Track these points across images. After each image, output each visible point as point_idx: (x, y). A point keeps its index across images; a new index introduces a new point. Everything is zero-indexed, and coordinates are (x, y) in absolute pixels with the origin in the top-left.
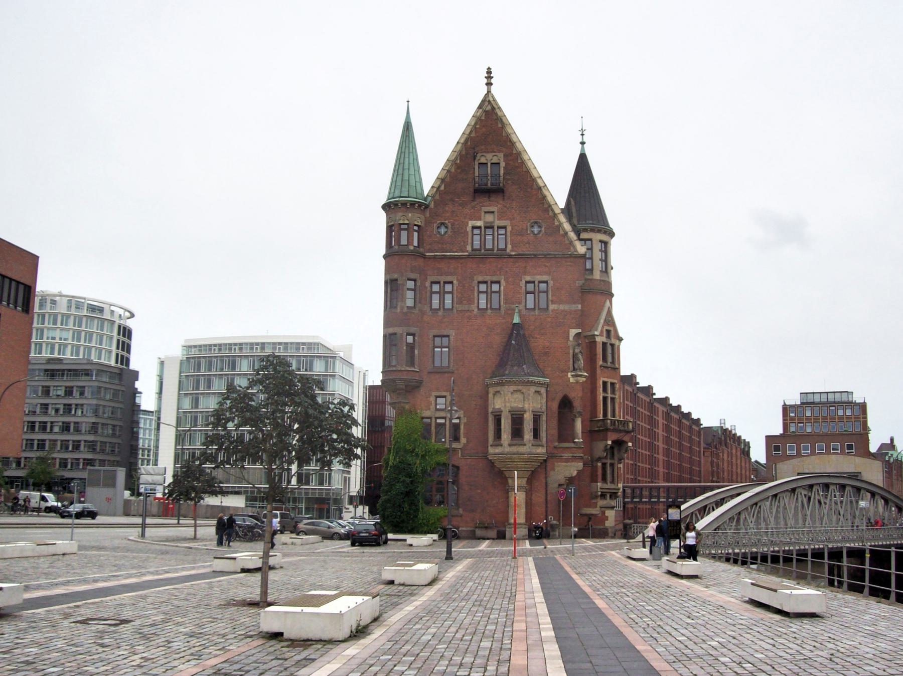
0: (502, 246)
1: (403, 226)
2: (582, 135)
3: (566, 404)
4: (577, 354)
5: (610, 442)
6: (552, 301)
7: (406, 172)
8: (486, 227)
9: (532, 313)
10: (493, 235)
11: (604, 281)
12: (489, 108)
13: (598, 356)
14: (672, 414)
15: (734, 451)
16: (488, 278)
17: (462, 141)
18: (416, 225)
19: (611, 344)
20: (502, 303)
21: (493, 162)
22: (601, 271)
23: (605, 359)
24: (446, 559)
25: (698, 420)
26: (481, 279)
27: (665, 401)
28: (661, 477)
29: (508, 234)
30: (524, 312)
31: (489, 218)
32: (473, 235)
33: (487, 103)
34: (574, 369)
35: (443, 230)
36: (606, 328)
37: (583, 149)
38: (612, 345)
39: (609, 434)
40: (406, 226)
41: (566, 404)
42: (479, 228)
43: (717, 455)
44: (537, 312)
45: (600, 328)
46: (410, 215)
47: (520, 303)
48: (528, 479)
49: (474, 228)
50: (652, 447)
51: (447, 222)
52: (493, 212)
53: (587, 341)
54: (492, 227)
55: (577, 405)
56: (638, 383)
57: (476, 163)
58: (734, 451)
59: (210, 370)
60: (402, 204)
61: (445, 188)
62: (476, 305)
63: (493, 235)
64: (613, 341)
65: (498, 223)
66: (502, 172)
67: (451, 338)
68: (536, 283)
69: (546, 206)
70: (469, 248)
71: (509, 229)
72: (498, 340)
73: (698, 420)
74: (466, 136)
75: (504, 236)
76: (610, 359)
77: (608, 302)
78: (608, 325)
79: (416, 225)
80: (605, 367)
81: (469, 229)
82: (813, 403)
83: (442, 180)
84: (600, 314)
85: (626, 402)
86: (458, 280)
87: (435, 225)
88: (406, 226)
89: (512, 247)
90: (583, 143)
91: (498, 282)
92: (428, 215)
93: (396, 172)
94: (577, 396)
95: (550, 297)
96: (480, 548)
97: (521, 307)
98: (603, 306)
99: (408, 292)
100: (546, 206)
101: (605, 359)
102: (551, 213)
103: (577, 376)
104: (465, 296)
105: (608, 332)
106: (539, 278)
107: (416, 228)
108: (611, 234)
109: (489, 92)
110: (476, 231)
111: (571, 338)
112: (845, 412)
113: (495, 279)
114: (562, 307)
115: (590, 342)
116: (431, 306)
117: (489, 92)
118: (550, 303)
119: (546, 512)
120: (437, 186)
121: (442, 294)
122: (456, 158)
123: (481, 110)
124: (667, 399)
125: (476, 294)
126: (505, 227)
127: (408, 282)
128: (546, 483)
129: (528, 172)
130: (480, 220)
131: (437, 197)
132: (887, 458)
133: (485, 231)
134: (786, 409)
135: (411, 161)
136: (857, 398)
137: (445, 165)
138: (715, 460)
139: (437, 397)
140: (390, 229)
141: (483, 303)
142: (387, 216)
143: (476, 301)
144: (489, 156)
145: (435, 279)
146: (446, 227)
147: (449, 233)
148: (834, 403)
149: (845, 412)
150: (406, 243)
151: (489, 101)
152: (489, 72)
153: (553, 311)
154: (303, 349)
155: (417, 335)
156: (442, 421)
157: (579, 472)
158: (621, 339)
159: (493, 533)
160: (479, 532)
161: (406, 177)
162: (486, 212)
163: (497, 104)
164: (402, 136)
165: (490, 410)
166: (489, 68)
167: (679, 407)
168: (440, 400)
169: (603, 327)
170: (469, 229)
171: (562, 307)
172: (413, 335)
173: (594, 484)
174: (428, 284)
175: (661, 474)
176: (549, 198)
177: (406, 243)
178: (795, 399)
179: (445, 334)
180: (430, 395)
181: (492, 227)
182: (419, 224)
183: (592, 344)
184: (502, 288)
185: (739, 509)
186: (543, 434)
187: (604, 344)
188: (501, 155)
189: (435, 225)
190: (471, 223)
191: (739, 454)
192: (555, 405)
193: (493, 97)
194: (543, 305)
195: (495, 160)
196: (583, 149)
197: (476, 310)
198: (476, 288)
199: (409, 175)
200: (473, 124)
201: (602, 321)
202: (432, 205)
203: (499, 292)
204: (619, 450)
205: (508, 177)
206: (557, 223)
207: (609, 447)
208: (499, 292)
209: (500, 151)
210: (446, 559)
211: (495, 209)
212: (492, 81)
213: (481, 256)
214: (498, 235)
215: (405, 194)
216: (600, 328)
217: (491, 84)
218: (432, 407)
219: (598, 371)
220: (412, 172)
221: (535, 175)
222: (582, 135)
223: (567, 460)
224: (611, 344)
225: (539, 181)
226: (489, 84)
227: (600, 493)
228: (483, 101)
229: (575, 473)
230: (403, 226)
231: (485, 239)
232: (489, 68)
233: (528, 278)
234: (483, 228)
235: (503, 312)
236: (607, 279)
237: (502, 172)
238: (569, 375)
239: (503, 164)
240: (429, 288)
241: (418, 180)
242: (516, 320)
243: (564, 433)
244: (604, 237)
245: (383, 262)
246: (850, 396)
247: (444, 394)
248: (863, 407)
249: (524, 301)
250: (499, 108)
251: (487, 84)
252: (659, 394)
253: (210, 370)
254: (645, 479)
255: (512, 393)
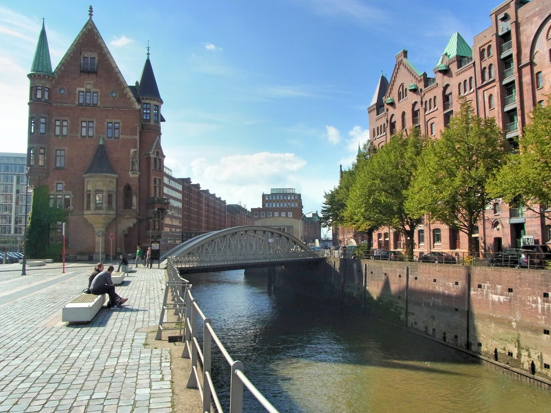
0: (95, 102)
1: (39, 88)
2: (148, 50)
3: (128, 188)
4: (134, 162)
5: (156, 209)
6: (121, 133)
7: (41, 57)
8: (86, 92)
9: (110, 139)
10: (90, 96)
11: (156, 126)
12: (90, 27)
13: (151, 165)
14: (217, 201)
15: (243, 216)
16: (87, 119)
17: (74, 44)
18: (46, 88)
19: (159, 159)
20: (94, 133)
21: (91, 57)
22: (155, 121)
23: (155, 167)
24: (22, 275)
25: (225, 201)
26: (83, 120)
27: (207, 192)
28: (204, 228)
29: (99, 96)
30: (106, 139)
31: (89, 87)
32: (79, 95)
33: (89, 25)
34: (132, 170)
35: (62, 92)
36: (156, 150)
37: (148, 57)
38: (160, 160)
39: (156, 205)
40: (40, 88)
41: (128, 188)
42: (83, 92)
43: (235, 218)
44: (113, 139)
45: (153, 150)
46: (43, 82)
47: (104, 134)
48: (106, 228)
49: (79, 92)
50: (199, 214)
51: (65, 87)
52: (91, 84)
53: (146, 157)
54: (90, 92)
55: (134, 188)
56: (191, 182)
57: (82, 56)
58: (243, 216)
59: (7, 181)
60: (38, 75)
61: (64, 69)
62: (80, 134)
63: (90, 96)
64: (160, 157)
65: (93, 90)
66: (96, 62)
67: (66, 151)
68: (113, 123)
69: (120, 83)
70: (77, 103)
71: (99, 93)
72: (91, 153)
73: (225, 201)
74: (76, 41)
75: (96, 97)
76: (158, 167)
77: (158, 137)
78: (158, 149)
79: (46, 88)
80: (155, 170)
81: (77, 92)
82: (280, 194)
83: (61, 64)
84: (153, 143)
85: (185, 191)
86: (70, 119)
87: (58, 88)
88: (40, 88)
89: (101, 103)
90: (148, 54)
91: (92, 122)
92: (54, 82)
93: (38, 60)
94: (134, 185)
95: (120, 131)
96: (355, 268)
97: (105, 136)
98: (155, 139)
99: (41, 124)
100: (120, 83)
101: (155, 167)
102: (122, 87)
103: (134, 173)
104: (74, 128)
105: (158, 153)
106: (114, 121)
107: (47, 89)
108: (162, 102)
109: (91, 19)
110: (81, 94)
111: (131, 154)
112: (291, 198)
113: (90, 120)
114: (127, 137)
115: (148, 158)
116: (55, 133)
117: (91, 19)
118: (120, 134)
119: (116, 246)
120: (59, 67)
121: (61, 126)
122: (71, 53)
123: (85, 28)
124: (208, 190)
125: (80, 128)
126: (97, 93)
127: (41, 119)
128: (116, 230)
129: (110, 64)
130: (83, 87)
131: (60, 73)
132: (314, 220)
133: (86, 94)
134: (264, 196)
135: (44, 52)
136: (297, 192)
137: (65, 56)
138: (233, 220)
139: (57, 184)
140: (31, 89)
141: (84, 133)
142: (31, 84)
143: (80, 132)
144: (89, 53)
145: (57, 118)
146: (64, 90)
147: (66, 93)
148: (286, 194)
149: (291, 198)
150: (40, 97)
151: (90, 24)
152: (91, 8)
153: (122, 138)
154: (5, 160)
155: (46, 148)
156: (60, 197)
157: (134, 225)
158: (164, 157)
159: (86, 257)
160: (79, 257)
161: (41, 61)
162: (86, 84)
163: (95, 26)
164: (40, 38)
165: (85, 191)
166: (91, 6)
167: (214, 195)
168: (59, 185)
169: (155, 149)
170: (77, 92)
171: (127, 137)
172: (44, 149)
173: (148, 231)
174: (53, 121)
175: (204, 227)
176: (121, 79)
177: (40, 97)
178: (268, 192)
179: (63, 149)
180: (53, 183)
181: (90, 92)
182: (49, 87)
183: (149, 159)
184: (94, 125)
185: (203, 242)
186: (114, 205)
187: (155, 159)
188: (96, 54)
189: (58, 88)
190: (78, 89)
191: (245, 217)
192: (121, 189)
193: (92, 22)
194: (116, 136)
195: (93, 56)
196: (148, 57)
197: (80, 136)
198: (80, 124)
199: (43, 59)
200: (81, 35)
201: (154, 147)
202: (56, 77)
203: (93, 127)
204: (162, 213)
205: (100, 65)
206: (125, 92)
207: (156, 212)
208: (93, 127)
209: (96, 52)
210: (22, 275)
211: (92, 82)
212: (93, 13)
213: (84, 106)
214: (93, 96)
215: (40, 70)
216: (153, 150)
217: (92, 15)
218: (55, 190)
219: (151, 172)
220: (45, 58)
221: (114, 66)
222: (148, 50)
223: (127, 219)
224: (159, 159)
225: (116, 69)
226: (91, 15)
227: (151, 236)
228: (87, 24)
229: (132, 225)
230: (39, 88)
231: (86, 98)
232: (91, 6)
233: (109, 121)
234: (85, 92)
235: (95, 138)
236: (157, 125)
237: (96, 62)
238: (130, 173)
239: (97, 59)
240: (54, 123)
241: (48, 63)
242: (101, 143)
243: (128, 204)
244: (157, 103)
245: (28, 107)
246: (294, 191)
247: (61, 182)
248: (299, 196)
249: (106, 133)
250: (96, 28)
251: (89, 15)
252: (203, 188)
253: (7, 181)
254: (194, 229)
255: (96, 182)
